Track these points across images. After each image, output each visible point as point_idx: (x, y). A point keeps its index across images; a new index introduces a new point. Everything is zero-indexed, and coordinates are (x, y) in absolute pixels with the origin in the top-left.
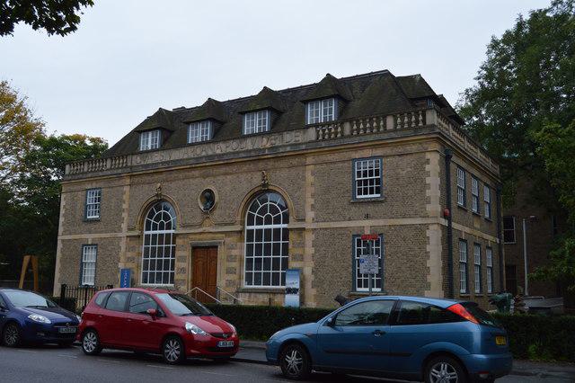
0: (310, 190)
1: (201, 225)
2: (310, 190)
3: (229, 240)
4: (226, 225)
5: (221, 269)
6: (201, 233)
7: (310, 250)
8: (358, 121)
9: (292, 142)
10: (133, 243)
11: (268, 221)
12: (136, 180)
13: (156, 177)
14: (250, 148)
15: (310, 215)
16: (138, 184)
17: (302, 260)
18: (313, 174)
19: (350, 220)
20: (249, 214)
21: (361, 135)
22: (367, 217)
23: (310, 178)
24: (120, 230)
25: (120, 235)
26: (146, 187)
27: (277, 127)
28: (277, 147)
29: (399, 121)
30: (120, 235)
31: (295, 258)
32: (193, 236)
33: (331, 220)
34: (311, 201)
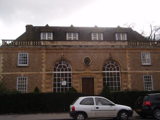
0: (128, 61)
1: (84, 70)
2: (128, 61)
3: (97, 76)
4: (96, 70)
5: (95, 86)
6: (85, 73)
7: (130, 79)
8: (141, 42)
9: (119, 45)
10: (49, 77)
11: (111, 70)
12: (49, 51)
13: (60, 51)
14: (103, 45)
15: (129, 68)
16: (50, 52)
17: (127, 82)
18: (128, 56)
19: (142, 70)
20: (54, 68)
21: (34, 46)
22: (147, 70)
23: (128, 57)
24: (42, 71)
25: (41, 73)
26: (55, 54)
27: (56, 39)
28: (114, 46)
29: (34, 43)
30: (41, 73)
31: (124, 82)
32: (81, 74)
33: (136, 70)
34: (129, 64)
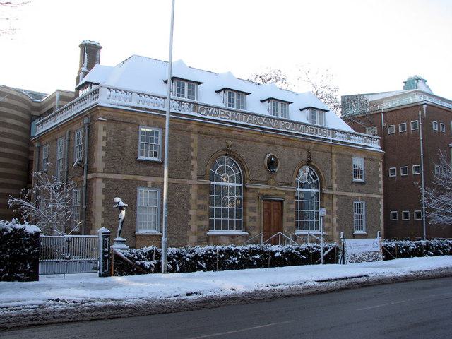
0: (334, 171)
15: (335, 186)
25: (189, 182)
